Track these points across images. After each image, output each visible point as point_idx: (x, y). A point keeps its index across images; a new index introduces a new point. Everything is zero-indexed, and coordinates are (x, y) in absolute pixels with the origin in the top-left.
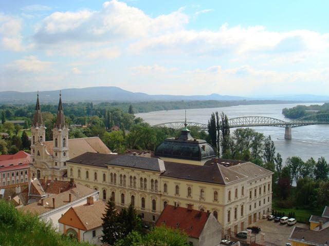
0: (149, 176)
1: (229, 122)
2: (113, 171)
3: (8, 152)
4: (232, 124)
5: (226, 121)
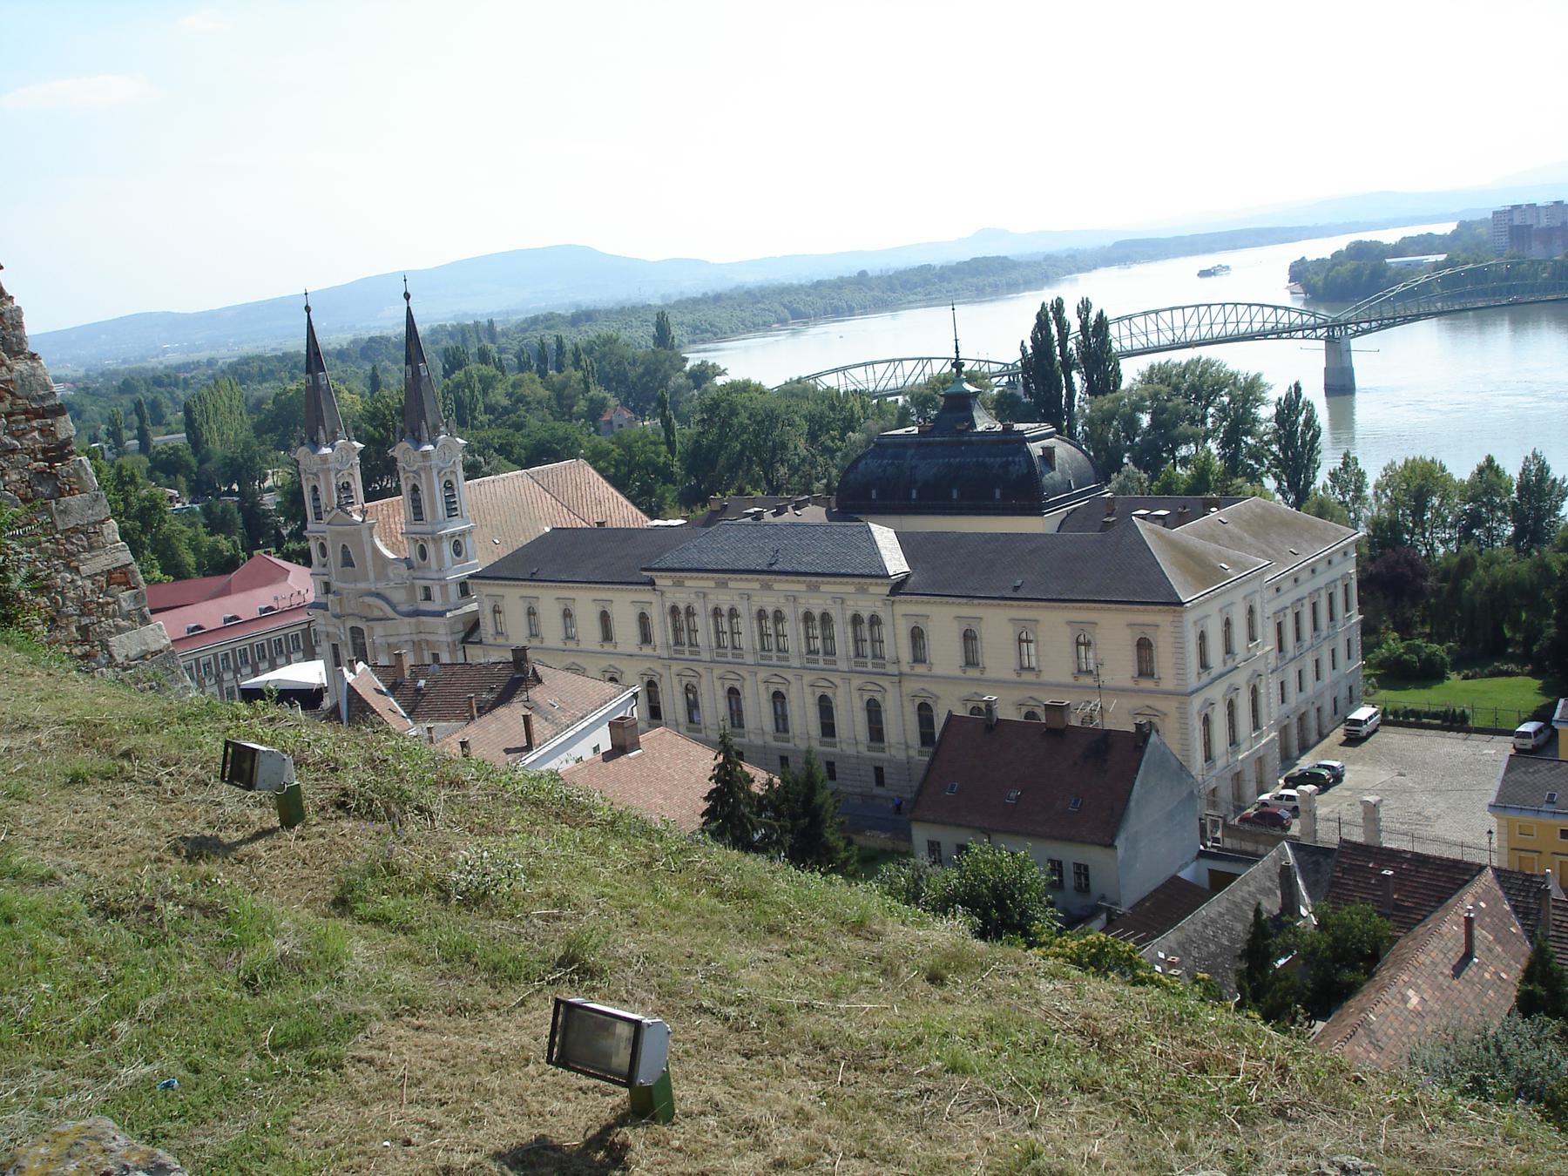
0: (842, 601)
1: (1113, 330)
2: (681, 598)
4: (1127, 344)
5: (1097, 330)
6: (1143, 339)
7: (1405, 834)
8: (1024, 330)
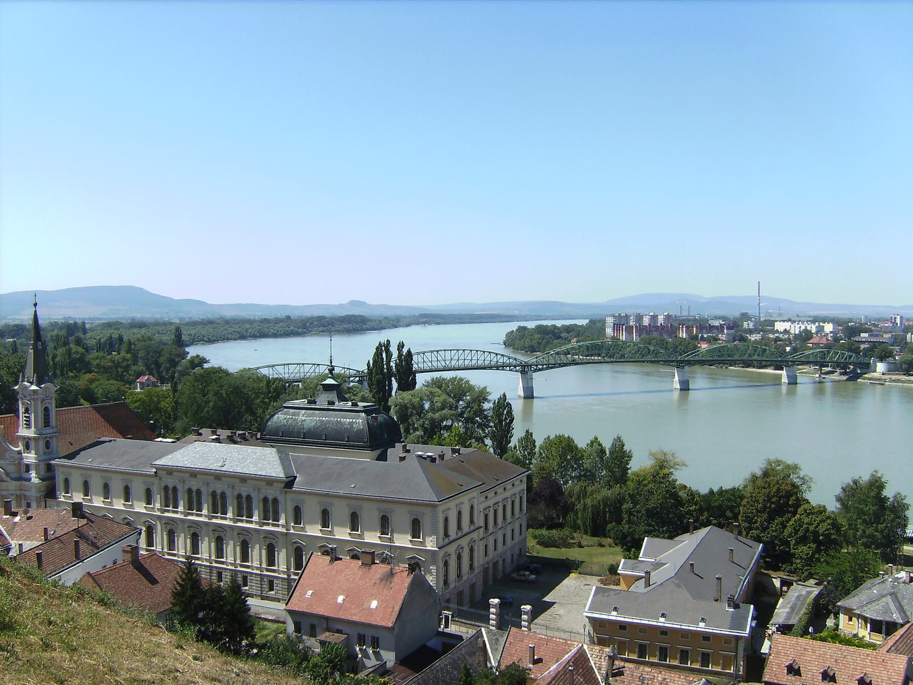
4: (421, 365)
6: (430, 364)
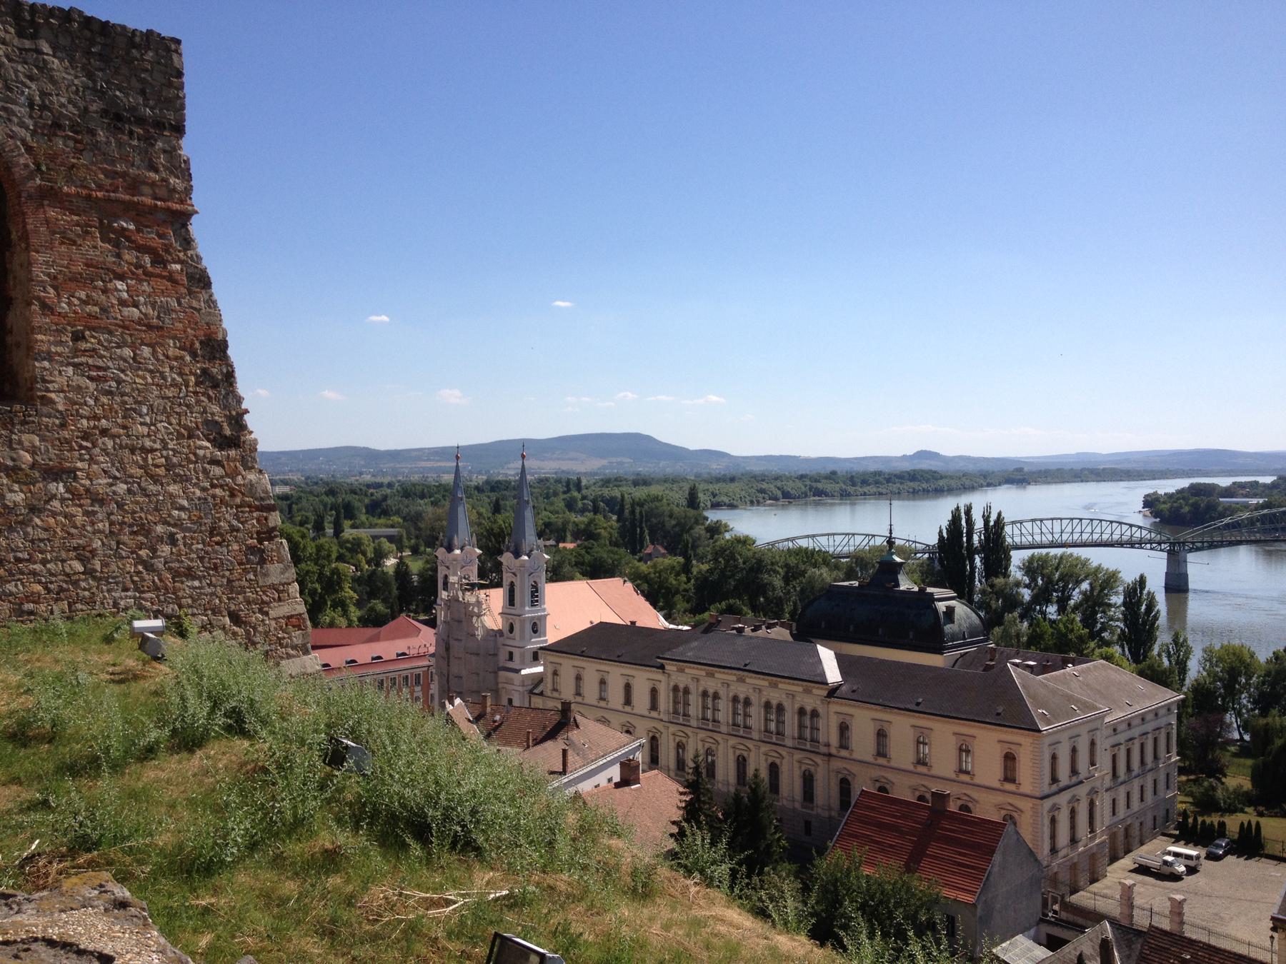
1: (1008, 529)
2: (682, 680)
3: (360, 619)
4: (1017, 540)
5: (995, 530)
6: (1030, 539)
7: (1204, 929)
8: (944, 520)
